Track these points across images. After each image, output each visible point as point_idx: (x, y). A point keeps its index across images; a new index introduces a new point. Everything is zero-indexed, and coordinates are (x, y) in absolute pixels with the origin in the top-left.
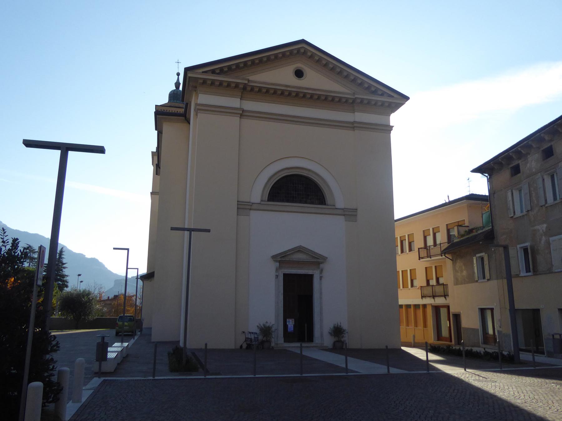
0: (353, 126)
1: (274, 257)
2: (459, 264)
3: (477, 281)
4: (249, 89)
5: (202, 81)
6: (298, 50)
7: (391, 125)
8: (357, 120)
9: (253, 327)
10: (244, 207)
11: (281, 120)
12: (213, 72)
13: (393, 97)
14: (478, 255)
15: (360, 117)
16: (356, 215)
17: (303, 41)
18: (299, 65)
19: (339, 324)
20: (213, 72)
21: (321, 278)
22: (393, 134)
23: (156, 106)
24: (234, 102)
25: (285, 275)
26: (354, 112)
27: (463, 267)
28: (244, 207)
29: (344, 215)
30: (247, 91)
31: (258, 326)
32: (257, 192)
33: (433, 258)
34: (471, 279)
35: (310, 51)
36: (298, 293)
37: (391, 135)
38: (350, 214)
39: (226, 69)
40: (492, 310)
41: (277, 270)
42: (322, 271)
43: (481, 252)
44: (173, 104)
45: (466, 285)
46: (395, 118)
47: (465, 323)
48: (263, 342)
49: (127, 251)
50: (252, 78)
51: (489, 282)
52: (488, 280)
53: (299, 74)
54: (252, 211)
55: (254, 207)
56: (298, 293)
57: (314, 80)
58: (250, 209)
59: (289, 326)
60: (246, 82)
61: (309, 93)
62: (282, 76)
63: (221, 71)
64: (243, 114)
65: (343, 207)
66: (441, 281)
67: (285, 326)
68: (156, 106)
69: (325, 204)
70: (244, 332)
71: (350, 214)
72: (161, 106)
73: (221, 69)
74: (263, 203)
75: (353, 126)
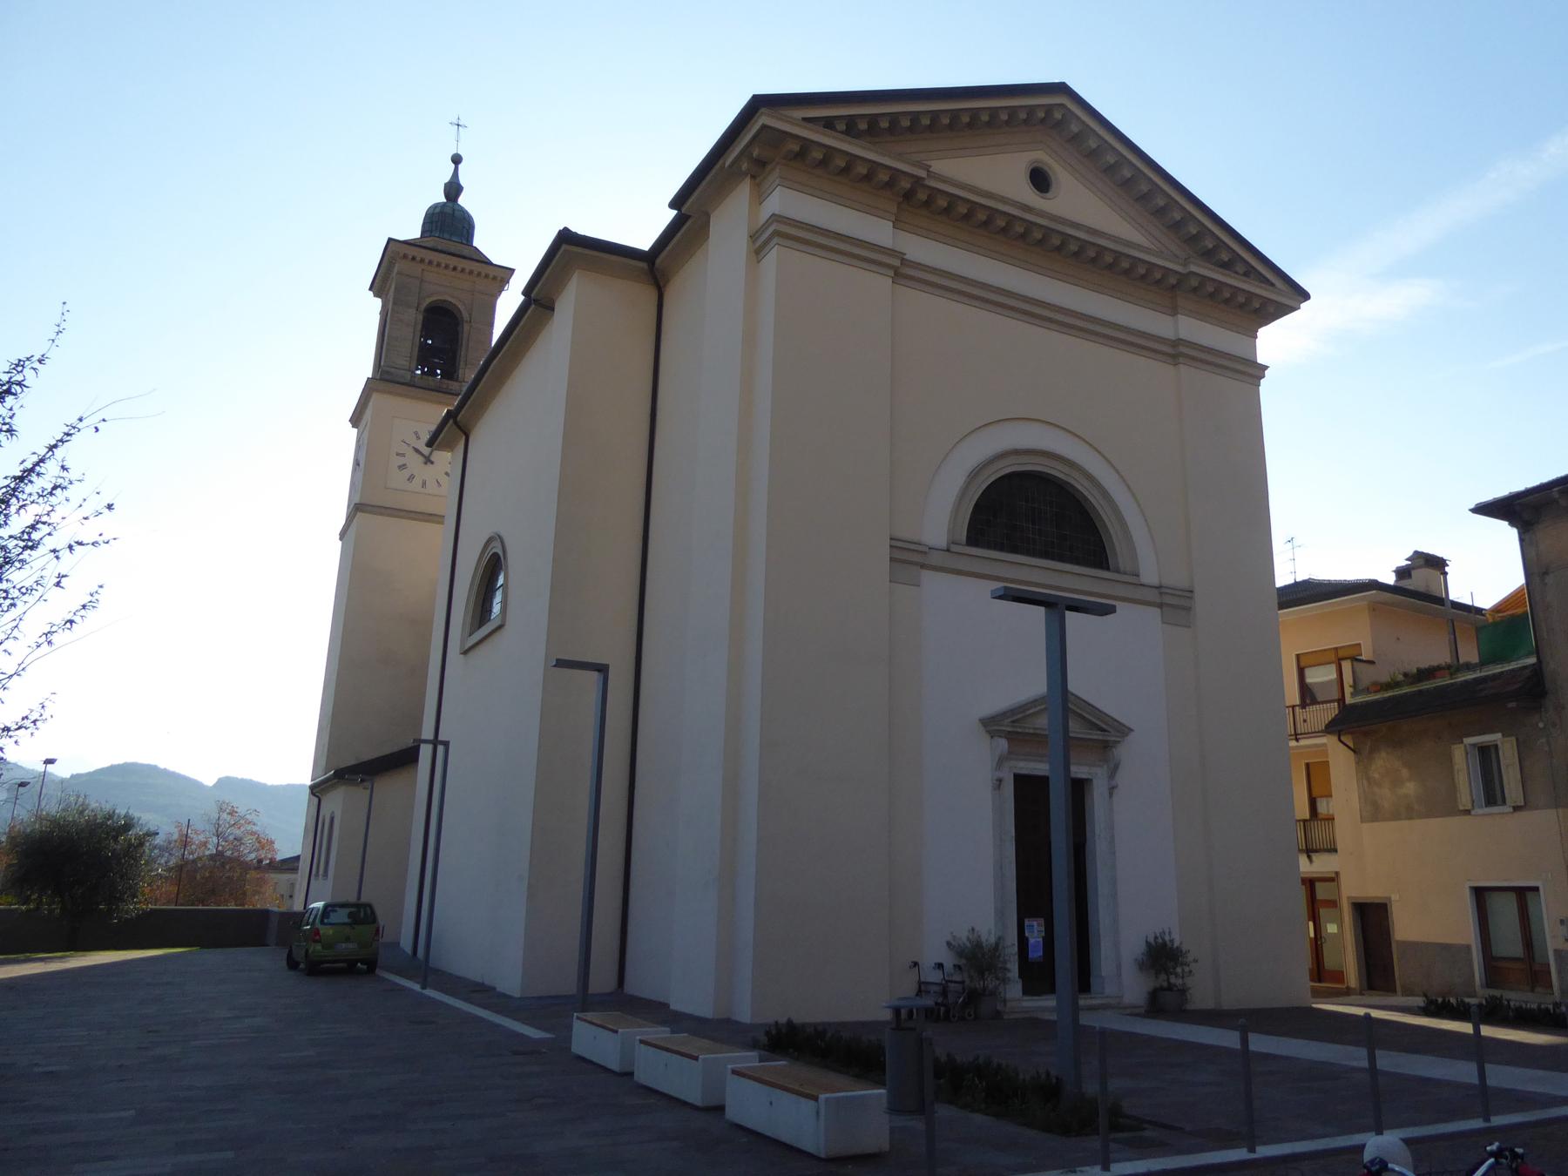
0: (1176, 352)
1: (991, 725)
2: (1383, 761)
3: (1468, 812)
4: (922, 196)
5: (796, 148)
6: (1049, 109)
7: (1260, 360)
8: (1183, 334)
9: (934, 952)
10: (908, 557)
11: (987, 301)
12: (829, 123)
13: (1272, 285)
14: (1469, 741)
15: (1193, 329)
16: (1188, 609)
17: (1062, 89)
18: (1040, 156)
19: (1167, 938)
20: (829, 123)
21: (1112, 789)
22: (1265, 387)
23: (390, 240)
24: (878, 230)
25: (1020, 780)
26: (1174, 311)
27: (1405, 772)
28: (908, 557)
29: (1160, 606)
30: (920, 203)
31: (948, 944)
32: (939, 515)
33: (1303, 742)
34: (1442, 805)
35: (1078, 118)
36: (1049, 833)
37: (1262, 389)
38: (1175, 603)
39: (863, 126)
40: (1523, 894)
41: (1001, 762)
42: (1114, 771)
43: (1492, 731)
44: (430, 242)
45: (1418, 822)
46: (1274, 342)
47: (1405, 927)
48: (973, 997)
49: (594, 676)
50: (939, 166)
51: (1517, 814)
52: (1516, 809)
53: (1040, 180)
54: (927, 576)
55: (936, 558)
56: (1049, 833)
57: (1078, 203)
58: (923, 566)
59: (1032, 941)
60: (923, 174)
61: (1078, 239)
62: (996, 174)
63: (851, 128)
64: (902, 271)
65: (1154, 581)
66: (1322, 807)
67: (1023, 941)
68: (390, 240)
69: (1108, 569)
70: (916, 964)
71: (1175, 603)
72: (406, 242)
73: (851, 121)
74: (954, 548)
75: (1176, 352)
